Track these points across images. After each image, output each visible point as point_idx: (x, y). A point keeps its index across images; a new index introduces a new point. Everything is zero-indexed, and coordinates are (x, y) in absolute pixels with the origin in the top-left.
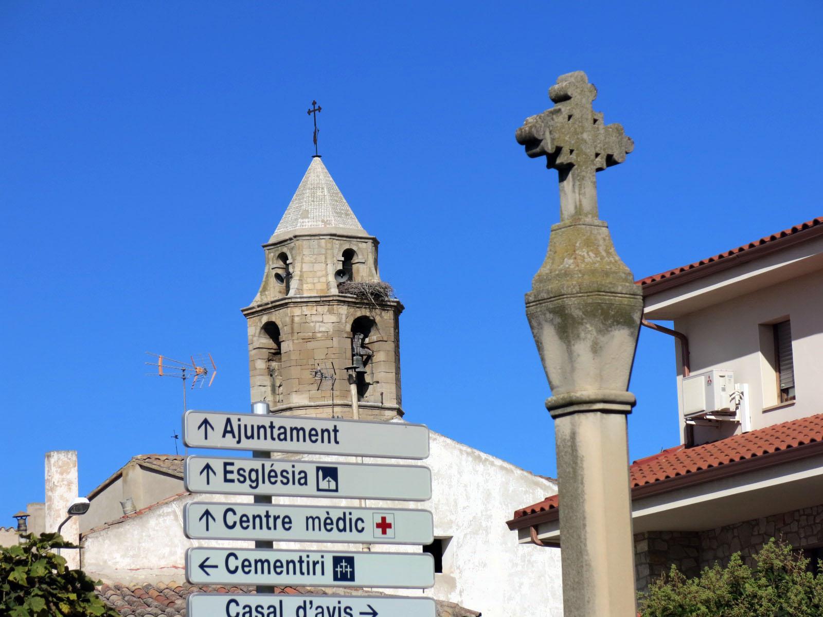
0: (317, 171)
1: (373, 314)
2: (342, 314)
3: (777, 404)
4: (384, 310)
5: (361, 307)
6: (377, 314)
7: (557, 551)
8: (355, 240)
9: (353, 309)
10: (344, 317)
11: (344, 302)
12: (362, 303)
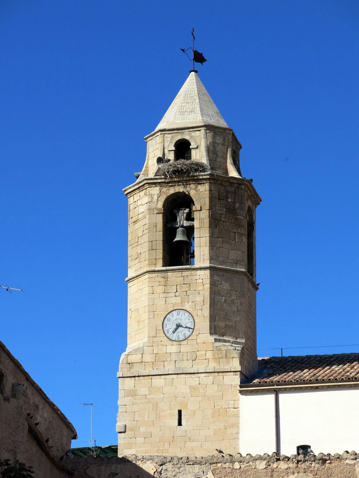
1: (188, 189)
2: (154, 195)
4: (200, 184)
6: (191, 189)
8: (187, 130)
10: (155, 197)
11: (155, 183)
12: (173, 181)
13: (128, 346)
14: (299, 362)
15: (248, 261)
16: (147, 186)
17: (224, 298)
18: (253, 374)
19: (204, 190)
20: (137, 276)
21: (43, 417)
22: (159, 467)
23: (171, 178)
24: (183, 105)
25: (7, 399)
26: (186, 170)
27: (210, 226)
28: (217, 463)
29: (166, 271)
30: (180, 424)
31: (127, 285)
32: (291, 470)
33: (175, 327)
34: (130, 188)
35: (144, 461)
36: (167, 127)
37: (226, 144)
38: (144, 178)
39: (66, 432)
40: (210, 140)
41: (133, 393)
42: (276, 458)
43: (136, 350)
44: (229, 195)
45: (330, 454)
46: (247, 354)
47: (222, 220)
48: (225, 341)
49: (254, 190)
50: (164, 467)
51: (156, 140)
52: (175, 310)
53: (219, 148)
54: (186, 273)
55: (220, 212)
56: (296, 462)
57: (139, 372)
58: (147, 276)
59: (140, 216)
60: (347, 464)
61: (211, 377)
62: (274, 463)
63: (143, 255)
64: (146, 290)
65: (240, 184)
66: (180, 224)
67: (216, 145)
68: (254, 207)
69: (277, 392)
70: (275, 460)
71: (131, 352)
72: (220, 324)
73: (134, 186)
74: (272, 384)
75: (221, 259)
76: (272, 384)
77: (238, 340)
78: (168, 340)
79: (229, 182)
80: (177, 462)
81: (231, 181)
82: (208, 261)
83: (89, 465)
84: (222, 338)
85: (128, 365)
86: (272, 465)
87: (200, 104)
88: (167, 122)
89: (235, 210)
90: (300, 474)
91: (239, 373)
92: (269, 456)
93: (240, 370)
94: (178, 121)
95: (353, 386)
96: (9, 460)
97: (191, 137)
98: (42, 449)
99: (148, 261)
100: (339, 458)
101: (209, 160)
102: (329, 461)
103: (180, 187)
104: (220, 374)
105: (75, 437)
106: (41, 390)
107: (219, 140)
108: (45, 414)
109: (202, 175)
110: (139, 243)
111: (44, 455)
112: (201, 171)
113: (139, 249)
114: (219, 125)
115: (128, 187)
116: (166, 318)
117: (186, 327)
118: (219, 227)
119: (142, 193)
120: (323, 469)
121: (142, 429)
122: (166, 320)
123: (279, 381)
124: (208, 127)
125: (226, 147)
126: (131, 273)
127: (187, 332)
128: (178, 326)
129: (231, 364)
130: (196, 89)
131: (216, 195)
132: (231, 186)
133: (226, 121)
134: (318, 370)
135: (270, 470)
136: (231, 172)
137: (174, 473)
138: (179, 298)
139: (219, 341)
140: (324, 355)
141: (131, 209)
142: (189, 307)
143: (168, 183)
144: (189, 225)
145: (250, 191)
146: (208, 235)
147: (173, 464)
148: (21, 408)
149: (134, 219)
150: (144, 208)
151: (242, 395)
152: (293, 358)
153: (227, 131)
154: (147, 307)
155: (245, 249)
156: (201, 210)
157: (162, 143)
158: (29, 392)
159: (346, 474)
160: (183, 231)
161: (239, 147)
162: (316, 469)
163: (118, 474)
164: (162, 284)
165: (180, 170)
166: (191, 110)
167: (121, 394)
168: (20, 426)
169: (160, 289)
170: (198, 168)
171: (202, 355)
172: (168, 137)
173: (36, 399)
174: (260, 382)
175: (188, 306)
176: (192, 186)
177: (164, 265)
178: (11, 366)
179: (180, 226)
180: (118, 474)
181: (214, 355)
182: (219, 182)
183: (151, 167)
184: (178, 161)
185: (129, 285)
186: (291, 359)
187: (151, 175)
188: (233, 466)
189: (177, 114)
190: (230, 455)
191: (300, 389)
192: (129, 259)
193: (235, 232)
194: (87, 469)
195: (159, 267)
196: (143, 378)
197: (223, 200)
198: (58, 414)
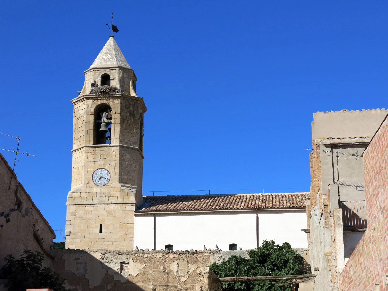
0: (110, 43)
1: (109, 102)
2: (89, 104)
3: (153, 217)
5: (101, 99)
7: (53, 242)
8: (109, 69)
9: (96, 101)
11: (90, 98)
13: (72, 188)
14: (164, 199)
15: (140, 143)
16: (85, 99)
18: (141, 205)
19: (117, 103)
20: (78, 149)
21: (40, 227)
22: (103, 255)
23: (99, 95)
24: (106, 55)
25: (23, 216)
26: (108, 91)
27: (120, 123)
28: (135, 254)
29: (95, 147)
30: (101, 232)
31: (72, 154)
32: (176, 258)
34: (75, 100)
35: (95, 252)
36: (97, 67)
38: (84, 95)
39: (50, 235)
40: (121, 75)
41: (74, 214)
42: (168, 252)
43: (77, 191)
45: (197, 250)
46: (138, 194)
47: (127, 119)
48: (127, 187)
49: (144, 104)
50: (106, 256)
51: (91, 74)
52: (100, 169)
53: (126, 80)
54: (106, 148)
55: (126, 115)
56: (178, 254)
57: (79, 202)
58: (84, 149)
59: (81, 116)
60: (206, 255)
61: (118, 207)
62: (166, 254)
63: (82, 137)
64: (84, 157)
65: (137, 100)
66: (103, 121)
67: (124, 78)
68: (143, 113)
69: (155, 216)
70: (167, 253)
72: (124, 178)
73: (77, 99)
74: (153, 211)
75: (126, 141)
76: (153, 211)
77: (134, 186)
78: (95, 185)
80: (113, 253)
81: (133, 98)
82: (119, 142)
83: (63, 254)
84: (125, 185)
85: (73, 198)
86: (165, 256)
87: (116, 55)
89: (134, 114)
90: (180, 261)
91: (134, 205)
92: (163, 250)
93: (135, 203)
94: (103, 64)
95: (197, 213)
96: (30, 250)
97: (111, 73)
98: (39, 244)
99: (85, 141)
100: (201, 252)
101: (121, 86)
102: (196, 254)
103: (104, 100)
104: (124, 205)
105: (54, 238)
106: (39, 211)
107: (126, 75)
108: (41, 225)
109: (117, 95)
110: (80, 130)
111: (40, 247)
112: (116, 92)
113: (80, 134)
115: (74, 99)
116: (94, 173)
117: (106, 178)
118: (125, 123)
119: (82, 103)
120: (193, 258)
121: (80, 234)
122: (94, 174)
123: (156, 210)
124: (120, 68)
125: (129, 79)
126: (74, 147)
127: (106, 181)
128: (101, 177)
129: (130, 200)
131: (124, 106)
132: (132, 101)
134: (176, 204)
135: (164, 258)
136: (132, 93)
137: (111, 259)
138: (102, 162)
140: (177, 196)
141: (75, 111)
142: (107, 167)
143: (98, 98)
144: (108, 122)
145: (142, 104)
146: (119, 128)
147: (111, 254)
148: (30, 221)
149: (77, 117)
150: (83, 111)
151: (136, 216)
152: (160, 197)
153: (131, 71)
154: (84, 167)
155: (138, 136)
156: (115, 114)
157: (94, 75)
158: (34, 212)
159: (205, 261)
160: (105, 125)
161: (136, 80)
162: (189, 258)
163: (80, 259)
164: (92, 154)
165: (105, 91)
166: (110, 58)
167: (68, 214)
168: (29, 231)
169: (91, 157)
170: (115, 90)
171: (114, 194)
172: (98, 72)
173: (37, 217)
174: (146, 210)
175: (106, 167)
176: (111, 100)
178: (26, 198)
179: (103, 122)
180: (80, 259)
181: (121, 194)
182: (126, 99)
183: (87, 89)
184: (104, 86)
185: (73, 154)
186: (159, 197)
187: (88, 93)
188: (144, 255)
189: (103, 60)
190: (142, 250)
191: (168, 214)
192: (74, 139)
193: (134, 127)
194: (62, 255)
195: (91, 144)
196: (80, 206)
197: (128, 108)
198: (47, 225)
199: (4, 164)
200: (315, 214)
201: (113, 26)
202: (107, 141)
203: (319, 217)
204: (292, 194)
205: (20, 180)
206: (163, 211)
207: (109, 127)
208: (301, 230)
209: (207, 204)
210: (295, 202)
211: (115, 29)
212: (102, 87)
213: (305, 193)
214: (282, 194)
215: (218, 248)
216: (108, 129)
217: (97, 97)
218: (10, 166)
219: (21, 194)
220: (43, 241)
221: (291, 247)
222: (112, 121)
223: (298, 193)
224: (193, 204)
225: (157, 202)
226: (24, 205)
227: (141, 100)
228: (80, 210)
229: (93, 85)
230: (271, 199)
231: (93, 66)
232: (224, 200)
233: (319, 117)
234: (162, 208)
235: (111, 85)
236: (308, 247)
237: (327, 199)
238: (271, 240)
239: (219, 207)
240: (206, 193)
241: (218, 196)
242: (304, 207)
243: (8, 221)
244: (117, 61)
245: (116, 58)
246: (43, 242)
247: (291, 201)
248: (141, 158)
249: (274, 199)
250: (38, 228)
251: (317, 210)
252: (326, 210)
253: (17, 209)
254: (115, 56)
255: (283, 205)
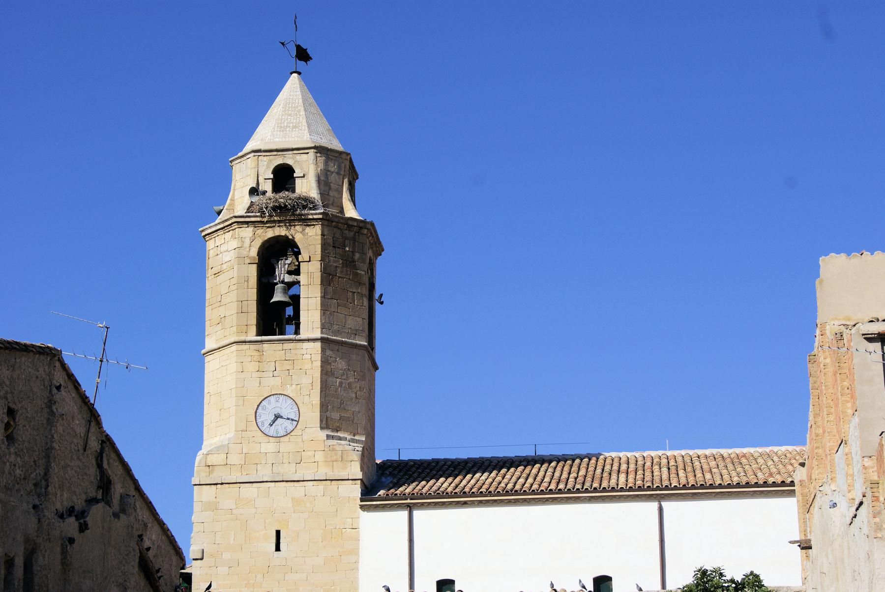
0: (293, 88)
1: (292, 231)
6: (297, 231)
10: (247, 241)
11: (247, 223)
13: (205, 443)
14: (426, 468)
17: (338, 380)
23: (270, 216)
25: (116, 515)
30: (278, 549)
33: (273, 418)
36: (263, 148)
37: (342, 173)
39: (174, 558)
40: (321, 166)
41: (213, 507)
43: (219, 449)
44: (347, 242)
46: (368, 453)
48: (340, 439)
49: (377, 235)
53: (333, 178)
54: (288, 346)
58: (234, 347)
59: (225, 266)
64: (233, 367)
65: (361, 228)
69: (410, 508)
71: (211, 450)
73: (216, 225)
75: (335, 327)
76: (404, 496)
77: (357, 438)
79: (347, 224)
81: (350, 223)
82: (319, 330)
84: (336, 434)
88: (262, 140)
89: (354, 262)
98: (150, 583)
107: (333, 167)
109: (312, 214)
112: (311, 209)
113: (222, 311)
114: (333, 147)
117: (288, 419)
119: (228, 235)
121: (226, 556)
124: (320, 150)
126: (210, 344)
127: (289, 426)
128: (277, 417)
130: (300, 97)
131: (330, 241)
133: (341, 141)
138: (278, 379)
139: (333, 437)
146: (319, 295)
148: (132, 527)
149: (215, 270)
153: (344, 156)
154: (234, 391)
155: (366, 315)
167: (197, 507)
169: (253, 367)
176: (298, 228)
177: (258, 334)
178: (120, 470)
183: (239, 201)
187: (240, 210)
192: (207, 324)
195: (252, 335)
198: (167, 536)
199: (74, 391)
200: (831, 503)
201: (299, 48)
202: (290, 328)
203: (845, 510)
204: (738, 451)
205: (109, 426)
206: (429, 496)
207: (292, 291)
208: (790, 542)
209: (535, 479)
210: (750, 473)
211: (303, 55)
212: (277, 197)
213: (771, 448)
214: (714, 451)
215: (584, 587)
216: (291, 297)
217: (265, 220)
218: (88, 394)
219: (111, 461)
220: (159, 575)
221: (765, 583)
222: (302, 278)
223: (752, 450)
224: (499, 478)
225: (411, 476)
226: (118, 489)
227: (369, 226)
228: (227, 497)
229: (254, 191)
230: (688, 464)
231: (250, 146)
232: (575, 468)
233: (835, 268)
234: (426, 488)
235: (299, 190)
236: (803, 584)
237: (873, 467)
238: (715, 566)
239: (566, 485)
240: (529, 452)
241: (559, 459)
242: (792, 483)
243: (83, 528)
244: (310, 132)
245: (308, 127)
246: (160, 578)
247: (739, 469)
248: (371, 368)
249: (697, 463)
250: (147, 543)
251: (835, 493)
252: (876, 494)
253: (103, 499)
254: (305, 120)
255: (722, 479)
